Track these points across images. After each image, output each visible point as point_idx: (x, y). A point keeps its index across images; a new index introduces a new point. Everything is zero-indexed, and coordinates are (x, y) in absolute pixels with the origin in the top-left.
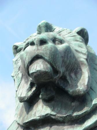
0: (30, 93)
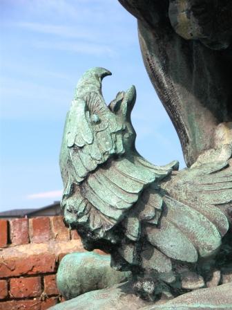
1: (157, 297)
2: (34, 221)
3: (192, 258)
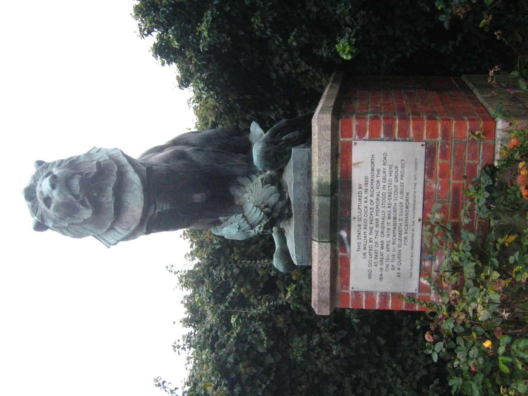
0: (90, 206)
1: (290, 210)
2: (342, 138)
3: (278, 195)
